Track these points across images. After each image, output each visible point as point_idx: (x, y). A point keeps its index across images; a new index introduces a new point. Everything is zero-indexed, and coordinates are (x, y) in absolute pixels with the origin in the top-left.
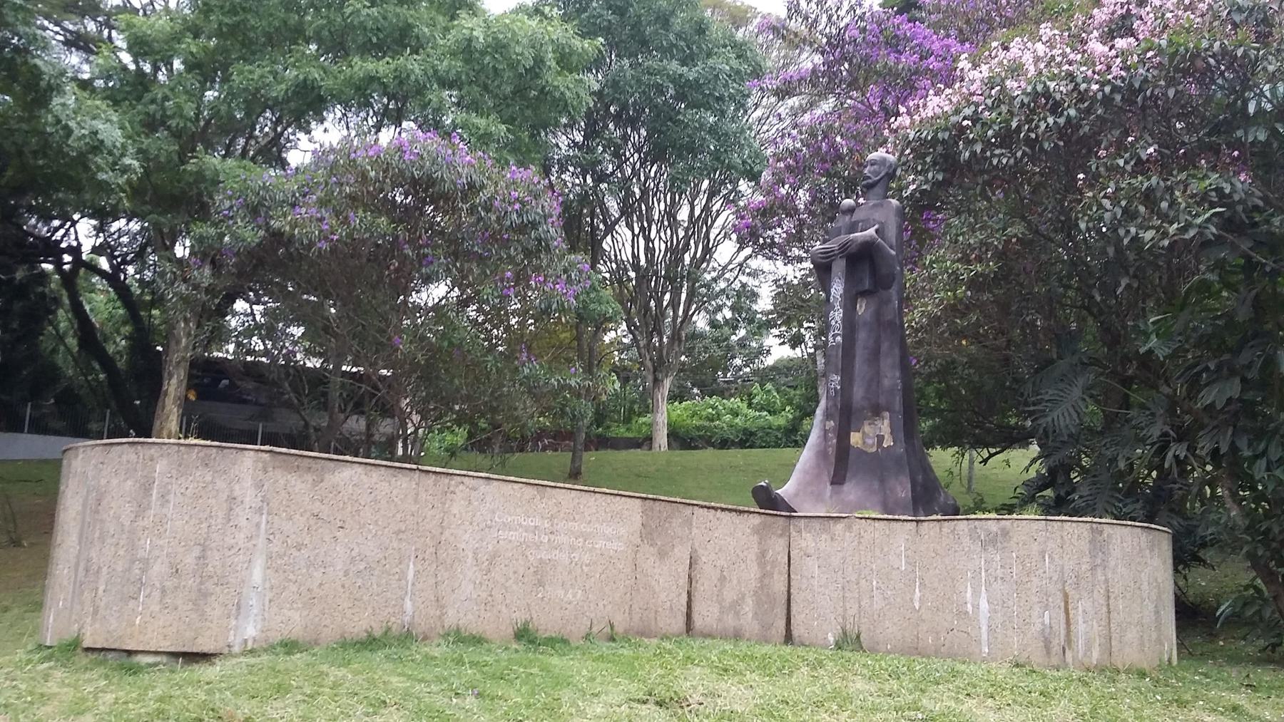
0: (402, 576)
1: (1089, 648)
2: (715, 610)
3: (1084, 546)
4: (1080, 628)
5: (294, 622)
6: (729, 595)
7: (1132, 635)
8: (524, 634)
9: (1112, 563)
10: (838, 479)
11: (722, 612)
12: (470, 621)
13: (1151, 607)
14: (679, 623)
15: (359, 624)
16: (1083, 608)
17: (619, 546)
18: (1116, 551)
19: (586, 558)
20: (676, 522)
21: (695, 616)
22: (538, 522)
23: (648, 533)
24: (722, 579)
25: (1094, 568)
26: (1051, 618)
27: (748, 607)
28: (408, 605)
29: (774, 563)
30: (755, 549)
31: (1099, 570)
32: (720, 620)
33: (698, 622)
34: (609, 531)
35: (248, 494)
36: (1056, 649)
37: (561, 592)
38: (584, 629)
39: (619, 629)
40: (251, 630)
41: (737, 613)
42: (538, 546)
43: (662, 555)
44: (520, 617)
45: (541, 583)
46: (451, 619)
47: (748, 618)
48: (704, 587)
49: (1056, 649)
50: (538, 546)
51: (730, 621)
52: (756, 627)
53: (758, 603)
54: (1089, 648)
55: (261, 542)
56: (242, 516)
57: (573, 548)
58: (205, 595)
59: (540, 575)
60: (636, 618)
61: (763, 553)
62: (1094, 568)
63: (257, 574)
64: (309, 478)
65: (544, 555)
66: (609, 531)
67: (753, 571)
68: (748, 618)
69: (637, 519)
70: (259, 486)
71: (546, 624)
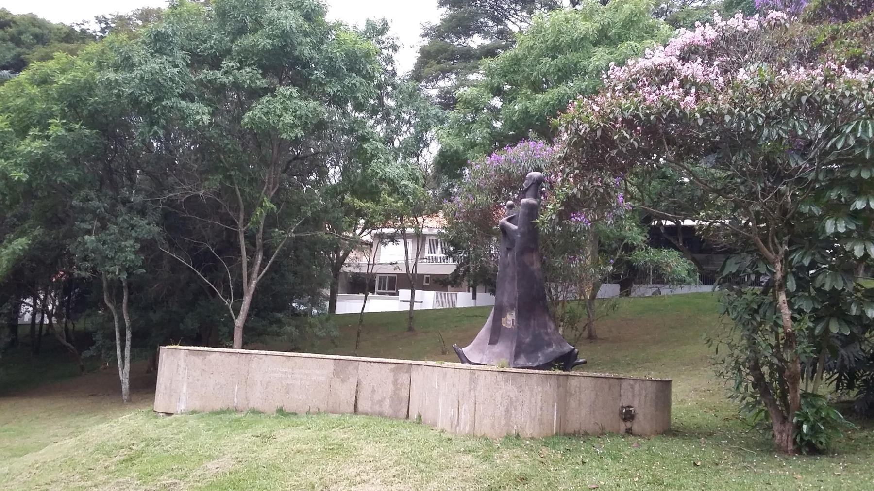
0: (233, 390)
3: (467, 380)
4: (463, 416)
5: (196, 405)
6: (377, 397)
7: (487, 421)
8: (281, 411)
9: (479, 388)
10: (493, 342)
11: (373, 405)
12: (259, 406)
14: (352, 408)
15: (218, 406)
16: (464, 407)
17: (324, 378)
18: (481, 382)
19: (308, 383)
20: (350, 368)
21: (359, 406)
23: (336, 373)
24: (374, 391)
25: (470, 390)
27: (387, 404)
28: (235, 400)
29: (402, 385)
30: (391, 378)
32: (371, 408)
33: (360, 408)
35: (183, 365)
37: (296, 396)
38: (306, 410)
39: (322, 410)
40: (182, 407)
41: (381, 406)
43: (343, 381)
44: (279, 405)
45: (288, 393)
46: (251, 405)
47: (387, 408)
48: (364, 394)
49: (454, 426)
51: (377, 408)
52: (391, 412)
53: (392, 401)
55: (185, 379)
56: (181, 370)
57: (302, 379)
58: (172, 396)
59: (288, 390)
60: (330, 406)
61: (396, 380)
64: (201, 358)
66: (318, 372)
67: (390, 388)
68: (387, 408)
69: (332, 368)
70: (185, 361)
71: (289, 408)
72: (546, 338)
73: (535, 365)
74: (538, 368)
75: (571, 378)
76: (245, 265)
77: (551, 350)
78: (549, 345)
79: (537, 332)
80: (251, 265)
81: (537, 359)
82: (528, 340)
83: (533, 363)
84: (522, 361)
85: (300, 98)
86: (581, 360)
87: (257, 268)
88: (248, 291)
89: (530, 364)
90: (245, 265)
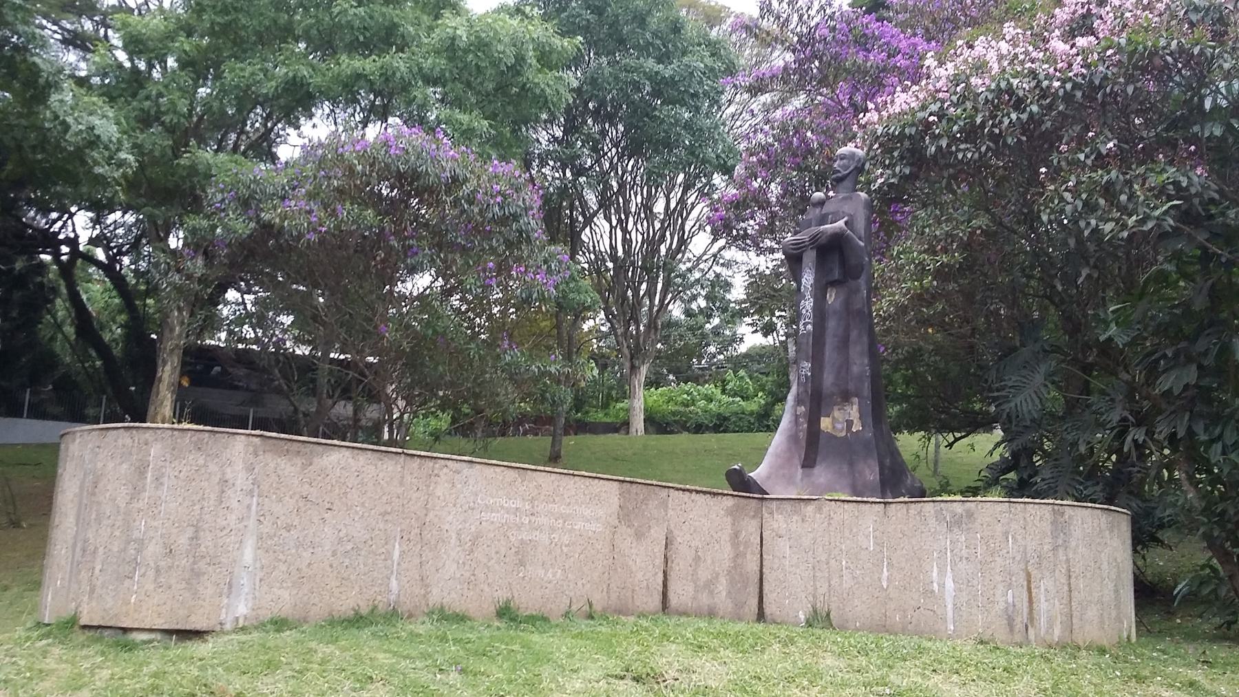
1: (1051, 626)
2: (691, 589)
3: (1047, 527)
4: (1042, 606)
5: (283, 601)
6: (704, 575)
7: (1092, 613)
8: (505, 612)
9: (1073, 544)
10: (809, 463)
13: (1111, 586)
14: (655, 601)
15: (347, 603)
17: (597, 527)
20: (653, 504)
21: (671, 595)
22: (519, 504)
23: (625, 514)
24: (697, 559)
25: (1055, 548)
26: (1015, 596)
27: (722, 587)
30: (729, 530)
31: (1061, 551)
33: (674, 600)
34: (587, 512)
35: (239, 477)
36: (1019, 626)
39: (597, 607)
40: (242, 609)
41: (711, 592)
42: (519, 527)
43: (639, 535)
45: (522, 563)
46: (435, 597)
47: (722, 597)
49: (1019, 626)
50: (519, 527)
51: (705, 599)
53: (732, 582)
54: (1051, 626)
56: (233, 498)
57: (553, 529)
59: (521, 556)
60: (614, 596)
62: (1055, 548)
63: (248, 555)
64: (299, 461)
65: (525, 536)
67: (727, 551)
68: (722, 597)
70: (250, 469)
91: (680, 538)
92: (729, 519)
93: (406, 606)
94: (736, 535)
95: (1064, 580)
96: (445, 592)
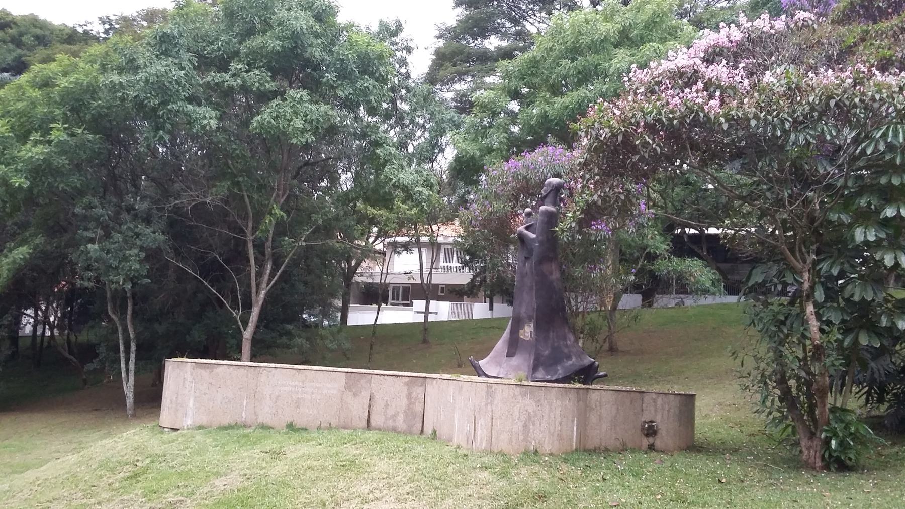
0: (242, 404)
1: (481, 442)
2: (383, 418)
3: (484, 394)
4: (479, 432)
5: (203, 420)
6: (391, 412)
7: (504, 437)
8: (290, 426)
9: (496, 402)
10: (510, 355)
13: (520, 424)
14: (364, 423)
15: (226, 421)
16: (481, 422)
17: (335, 392)
20: (363, 381)
21: (372, 421)
22: (297, 383)
23: (348, 387)
24: (387, 405)
25: (487, 405)
26: (469, 427)
27: (401, 418)
29: (416, 399)
30: (406, 392)
31: (489, 406)
33: (373, 423)
34: (329, 386)
35: (189, 378)
36: (470, 441)
39: (333, 425)
40: (189, 422)
41: (394, 420)
42: (297, 393)
43: (355, 395)
45: (298, 407)
46: (260, 420)
47: (400, 423)
49: (470, 441)
50: (297, 393)
51: (390, 423)
53: (406, 415)
54: (481, 442)
56: (187, 383)
57: (312, 393)
59: (298, 404)
60: (342, 421)
62: (487, 405)
63: (191, 403)
64: (208, 371)
65: (300, 396)
66: (329, 386)
67: (404, 402)
68: (400, 423)
70: (192, 374)
72: (566, 351)
73: (554, 379)
74: (556, 381)
75: (591, 392)
76: (253, 275)
77: (570, 362)
78: (569, 357)
79: (556, 344)
80: (259, 275)
81: (556, 372)
82: (547, 352)
83: (552, 376)
84: (540, 374)
85: (311, 102)
86: (601, 373)
87: (266, 278)
88: (257, 302)
89: (549, 377)
90: (253, 275)
91: (377, 396)
92: (406, 387)
93: (249, 422)
94: (410, 394)
95: (489, 420)
96: (264, 417)
